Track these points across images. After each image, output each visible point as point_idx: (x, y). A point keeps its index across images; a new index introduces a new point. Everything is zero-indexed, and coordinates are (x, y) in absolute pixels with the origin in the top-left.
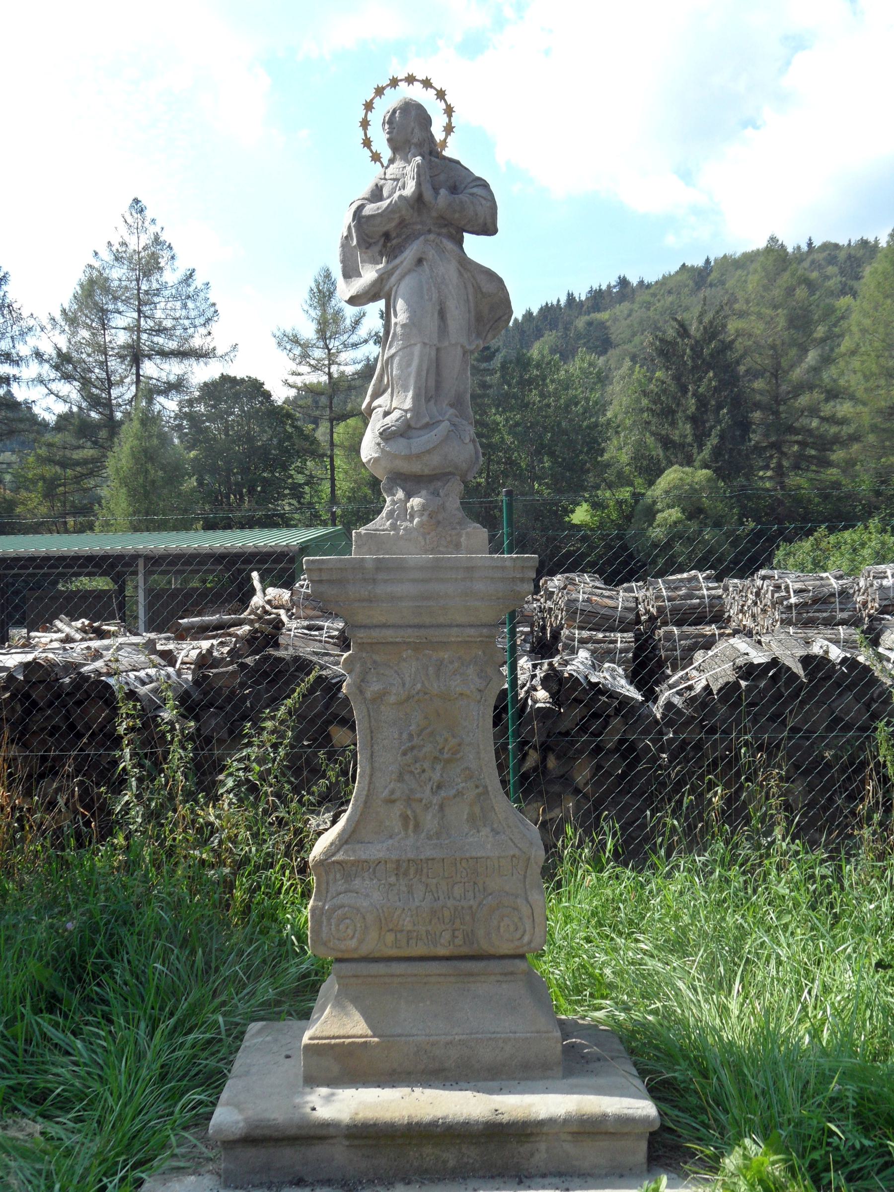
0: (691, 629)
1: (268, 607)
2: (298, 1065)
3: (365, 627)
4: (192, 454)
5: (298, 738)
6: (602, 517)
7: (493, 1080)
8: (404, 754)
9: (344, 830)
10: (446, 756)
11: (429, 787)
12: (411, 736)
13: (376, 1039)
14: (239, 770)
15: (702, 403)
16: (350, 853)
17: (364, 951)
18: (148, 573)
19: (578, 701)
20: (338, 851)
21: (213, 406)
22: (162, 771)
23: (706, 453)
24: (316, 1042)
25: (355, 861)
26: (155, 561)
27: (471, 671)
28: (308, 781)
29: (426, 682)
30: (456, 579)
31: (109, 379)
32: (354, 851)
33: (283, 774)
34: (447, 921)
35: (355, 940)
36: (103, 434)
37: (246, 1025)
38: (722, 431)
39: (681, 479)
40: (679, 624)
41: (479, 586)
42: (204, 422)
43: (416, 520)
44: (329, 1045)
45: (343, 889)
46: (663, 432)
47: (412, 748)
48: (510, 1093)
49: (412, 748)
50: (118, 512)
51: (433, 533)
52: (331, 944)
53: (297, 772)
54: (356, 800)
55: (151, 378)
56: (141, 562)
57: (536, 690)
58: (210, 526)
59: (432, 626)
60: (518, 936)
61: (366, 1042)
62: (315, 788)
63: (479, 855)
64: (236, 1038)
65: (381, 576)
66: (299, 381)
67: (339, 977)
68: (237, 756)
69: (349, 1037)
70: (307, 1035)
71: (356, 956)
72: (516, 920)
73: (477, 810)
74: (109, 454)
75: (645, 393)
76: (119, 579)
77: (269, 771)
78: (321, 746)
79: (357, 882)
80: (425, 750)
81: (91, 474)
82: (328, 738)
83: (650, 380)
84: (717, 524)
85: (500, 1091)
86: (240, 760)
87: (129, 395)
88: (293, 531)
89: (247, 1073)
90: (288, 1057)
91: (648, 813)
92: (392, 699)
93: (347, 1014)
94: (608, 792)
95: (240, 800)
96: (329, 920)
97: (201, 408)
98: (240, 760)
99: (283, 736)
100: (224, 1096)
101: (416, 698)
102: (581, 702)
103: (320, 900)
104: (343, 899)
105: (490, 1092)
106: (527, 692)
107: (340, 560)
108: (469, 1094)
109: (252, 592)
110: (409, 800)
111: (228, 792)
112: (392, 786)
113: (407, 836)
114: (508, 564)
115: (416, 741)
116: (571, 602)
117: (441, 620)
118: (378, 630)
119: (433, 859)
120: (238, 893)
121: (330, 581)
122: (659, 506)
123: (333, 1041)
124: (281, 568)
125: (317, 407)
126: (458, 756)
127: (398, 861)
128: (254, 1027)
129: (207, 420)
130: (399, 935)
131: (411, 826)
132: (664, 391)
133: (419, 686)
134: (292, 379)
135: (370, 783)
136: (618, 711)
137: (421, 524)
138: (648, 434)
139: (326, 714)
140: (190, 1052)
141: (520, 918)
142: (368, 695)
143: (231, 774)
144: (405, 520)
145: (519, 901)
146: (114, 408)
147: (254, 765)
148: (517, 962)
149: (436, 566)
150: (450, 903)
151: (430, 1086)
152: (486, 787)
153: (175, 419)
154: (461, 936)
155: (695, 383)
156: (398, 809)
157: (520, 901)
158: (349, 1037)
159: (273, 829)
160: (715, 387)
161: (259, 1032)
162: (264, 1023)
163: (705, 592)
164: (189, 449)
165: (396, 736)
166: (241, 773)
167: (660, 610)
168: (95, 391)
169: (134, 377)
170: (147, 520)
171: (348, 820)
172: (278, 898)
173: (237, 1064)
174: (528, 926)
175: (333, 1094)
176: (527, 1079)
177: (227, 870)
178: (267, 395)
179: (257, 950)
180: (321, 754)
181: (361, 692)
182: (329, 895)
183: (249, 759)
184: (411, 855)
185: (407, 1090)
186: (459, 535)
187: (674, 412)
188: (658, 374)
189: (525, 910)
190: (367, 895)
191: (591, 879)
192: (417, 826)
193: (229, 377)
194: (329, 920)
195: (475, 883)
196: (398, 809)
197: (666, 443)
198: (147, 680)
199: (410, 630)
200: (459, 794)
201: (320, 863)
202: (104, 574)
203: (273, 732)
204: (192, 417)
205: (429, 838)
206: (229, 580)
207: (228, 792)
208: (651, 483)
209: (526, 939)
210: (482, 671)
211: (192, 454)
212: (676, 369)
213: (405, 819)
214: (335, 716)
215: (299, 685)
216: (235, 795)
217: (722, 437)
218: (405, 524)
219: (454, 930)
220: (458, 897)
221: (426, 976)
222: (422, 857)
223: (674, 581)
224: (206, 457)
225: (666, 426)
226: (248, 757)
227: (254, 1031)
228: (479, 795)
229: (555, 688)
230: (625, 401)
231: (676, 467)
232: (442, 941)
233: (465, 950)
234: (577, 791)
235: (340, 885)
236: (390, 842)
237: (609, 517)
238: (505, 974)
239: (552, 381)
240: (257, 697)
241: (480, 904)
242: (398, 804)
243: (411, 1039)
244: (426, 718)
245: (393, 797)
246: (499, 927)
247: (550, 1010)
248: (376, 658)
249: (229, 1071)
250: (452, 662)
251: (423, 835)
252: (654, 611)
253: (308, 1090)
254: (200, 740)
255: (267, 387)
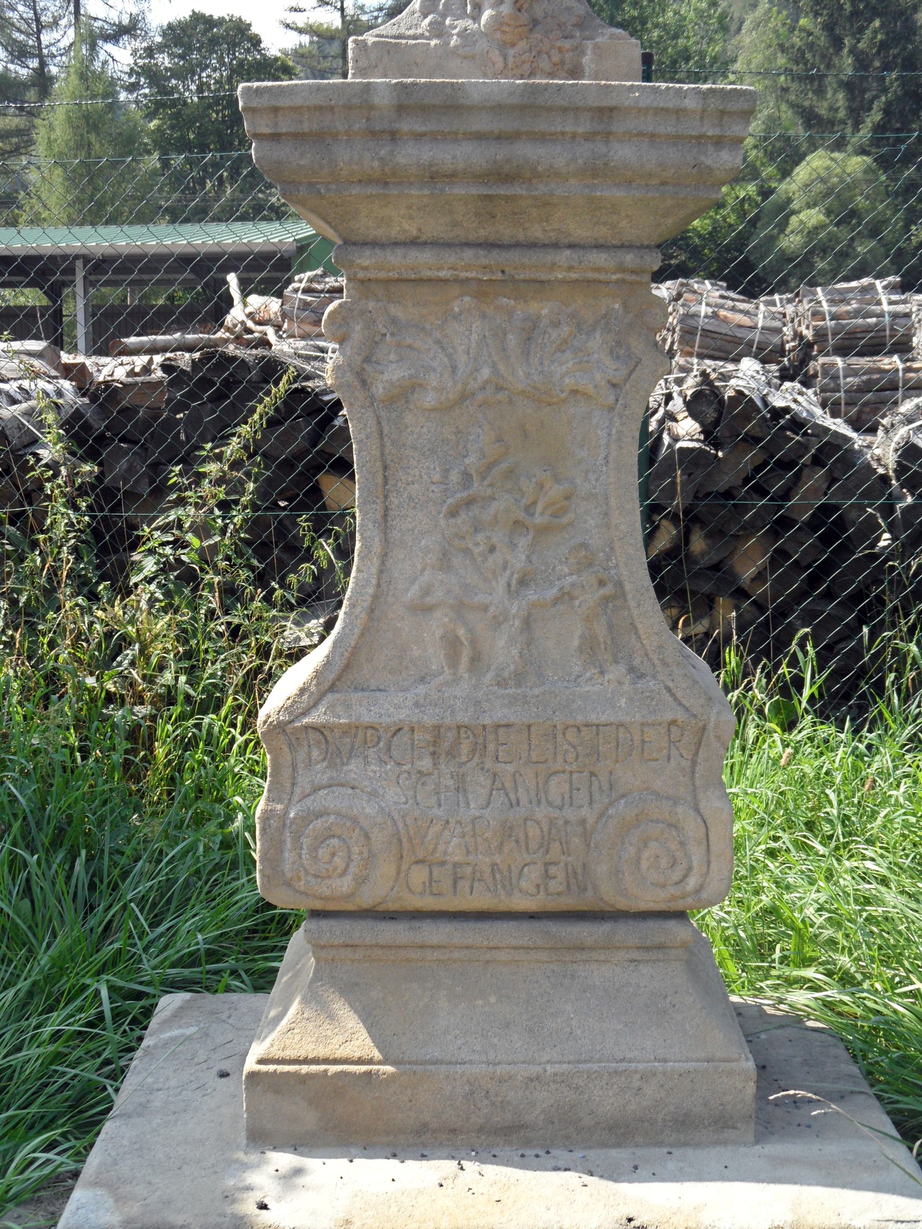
0: (864, 362)
1: (250, 324)
2: (237, 1106)
3: (374, 244)
4: (153, 124)
5: (262, 493)
6: (716, 221)
7: (618, 1145)
8: (453, 513)
9: (328, 663)
10: (538, 520)
11: (502, 581)
12: (467, 478)
13: (389, 1069)
14: (164, 544)
15: (862, 62)
16: (339, 709)
17: (366, 899)
18: (89, 283)
19: (752, 440)
20: (315, 705)
21: (182, 57)
22: (34, 545)
23: (865, 133)
24: (271, 1068)
25: (349, 725)
26: (100, 266)
27: (597, 343)
28: (282, 564)
29: (502, 368)
30: (574, 136)
31: (37, 20)
32: (348, 707)
33: (239, 553)
34: (533, 845)
35: (349, 878)
36: (32, 94)
37: (160, 997)
38: (889, 104)
39: (828, 168)
40: (843, 350)
41: (623, 153)
42: (169, 79)
43: (487, 14)
44: (296, 1074)
45: (325, 779)
46: (806, 103)
47: (469, 503)
48: (654, 1177)
49: (469, 503)
50: (52, 202)
51: (522, 45)
52: (301, 885)
53: (262, 551)
54: (352, 606)
55: (96, 19)
56: (79, 264)
57: (676, 420)
58: (176, 216)
59: (517, 245)
60: (676, 877)
61: (369, 1074)
62: (292, 578)
63: (603, 719)
64: (134, 1021)
65: (406, 125)
66: (300, 20)
67: (318, 947)
68: (160, 521)
69: (335, 1062)
70: (257, 1050)
71: (350, 907)
72: (674, 846)
73: (600, 629)
74: (38, 122)
75: (782, 48)
76: (54, 293)
77: (214, 549)
78: (303, 507)
79: (354, 767)
80: (495, 505)
81: (16, 151)
82: (316, 493)
83: (792, 29)
84: (874, 231)
85: (633, 1172)
86: (165, 529)
87: (65, 43)
88: (289, 225)
89: (143, 1109)
90: (224, 1075)
91: (865, 630)
92: (429, 399)
93: (332, 1017)
94: (801, 595)
95: (168, 594)
96: (297, 839)
97: (164, 60)
98: (165, 529)
99: (237, 488)
100: (94, 1159)
101: (480, 397)
102: (758, 440)
103: (280, 801)
104: (323, 799)
105: (613, 1174)
106: (661, 422)
107: (319, 88)
108: (572, 1178)
109: (230, 303)
110: (460, 608)
111: (149, 581)
112: (427, 577)
113: (456, 680)
114: (691, 103)
115: (477, 487)
116: (689, 317)
117: (536, 232)
118: (400, 251)
119: (507, 726)
120: (160, 751)
121: (298, 137)
122: (795, 205)
123: (305, 1069)
124: (268, 271)
125: (325, 57)
126: (569, 517)
127: (437, 728)
128: (169, 1003)
129: (172, 77)
130: (436, 872)
131: (465, 659)
132: (811, 46)
133: (486, 373)
134: (292, 18)
135: (381, 572)
136: (817, 461)
137: (497, 23)
138: (784, 107)
139: (308, 450)
140: (51, 1048)
141: (682, 844)
142: (379, 390)
143: (152, 552)
144: (463, 15)
145: (680, 809)
146: (49, 60)
147: (190, 537)
148: (672, 924)
149: (529, 105)
150: (542, 812)
151: (495, 1159)
152: (619, 584)
153: (130, 75)
154: (561, 876)
155: (853, 35)
156: (436, 626)
157: (683, 812)
158: (335, 1062)
159: (223, 643)
160: (881, 41)
161: (178, 1014)
162: (187, 996)
163: (886, 307)
164: (151, 116)
165: (437, 477)
166: (168, 550)
167: (820, 335)
168: (16, 35)
169: (72, 18)
170: (94, 212)
171: (335, 644)
172: (226, 759)
173: (130, 1083)
174: (697, 859)
175: (298, 1172)
176: (685, 1144)
177: (142, 710)
178: (256, 41)
179: (185, 853)
180: (303, 521)
181: (364, 383)
182: (298, 790)
183: (180, 526)
184: (463, 717)
185: (450, 1166)
186: (579, 51)
187: (821, 77)
188: (803, 22)
189: (692, 828)
190: (373, 794)
191: (776, 744)
192: (476, 660)
193: (203, 16)
194: (297, 839)
195: (592, 774)
196: (436, 626)
197: (810, 118)
198: (19, 397)
199: (469, 253)
200: (565, 597)
201: (278, 728)
202: (32, 284)
203: (219, 482)
204: (153, 75)
205: (501, 683)
206: (198, 289)
207: (149, 581)
208: (785, 173)
209: (692, 883)
210: (619, 343)
211: (153, 124)
212: (831, 15)
213: (452, 645)
214: (325, 455)
215: (261, 401)
216: (160, 586)
217: (887, 111)
218: (461, 24)
219: (547, 864)
220: (558, 802)
221: (491, 948)
222: (487, 721)
223: (840, 292)
224: (172, 127)
225: (810, 95)
226: (179, 524)
227: (167, 1013)
228: (606, 600)
229: (711, 415)
230: (758, 59)
231: (821, 152)
232: (523, 884)
233: (568, 903)
234: (741, 594)
235: (321, 773)
236: (421, 689)
237: (724, 220)
238: (647, 949)
239: (656, 26)
240: (193, 422)
241: (601, 815)
242: (438, 614)
243: (459, 1069)
244: (499, 440)
245: (429, 600)
246: (638, 860)
247: (712, 987)
248: (396, 311)
249: (117, 1090)
250: (556, 325)
251: (489, 677)
252: (809, 334)
253: (254, 1157)
254: (103, 494)
255: (254, 30)
